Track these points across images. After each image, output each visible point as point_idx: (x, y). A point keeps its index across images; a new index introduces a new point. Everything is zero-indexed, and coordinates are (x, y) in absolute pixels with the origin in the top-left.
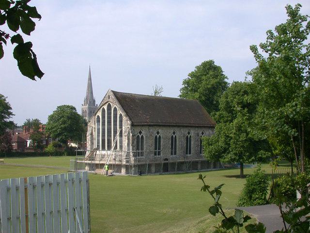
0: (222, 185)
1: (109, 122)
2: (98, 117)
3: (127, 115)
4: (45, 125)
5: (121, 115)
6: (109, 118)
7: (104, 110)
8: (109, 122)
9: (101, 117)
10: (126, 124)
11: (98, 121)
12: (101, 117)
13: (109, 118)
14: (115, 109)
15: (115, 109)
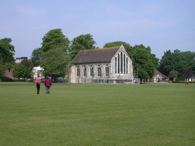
0: (38, 93)
1: (122, 60)
2: (116, 58)
3: (131, 57)
4: (150, 53)
5: (127, 58)
6: (122, 58)
7: (119, 54)
8: (122, 60)
9: (117, 58)
10: (130, 63)
11: (116, 59)
12: (117, 58)
13: (122, 58)
14: (124, 55)
15: (124, 55)
